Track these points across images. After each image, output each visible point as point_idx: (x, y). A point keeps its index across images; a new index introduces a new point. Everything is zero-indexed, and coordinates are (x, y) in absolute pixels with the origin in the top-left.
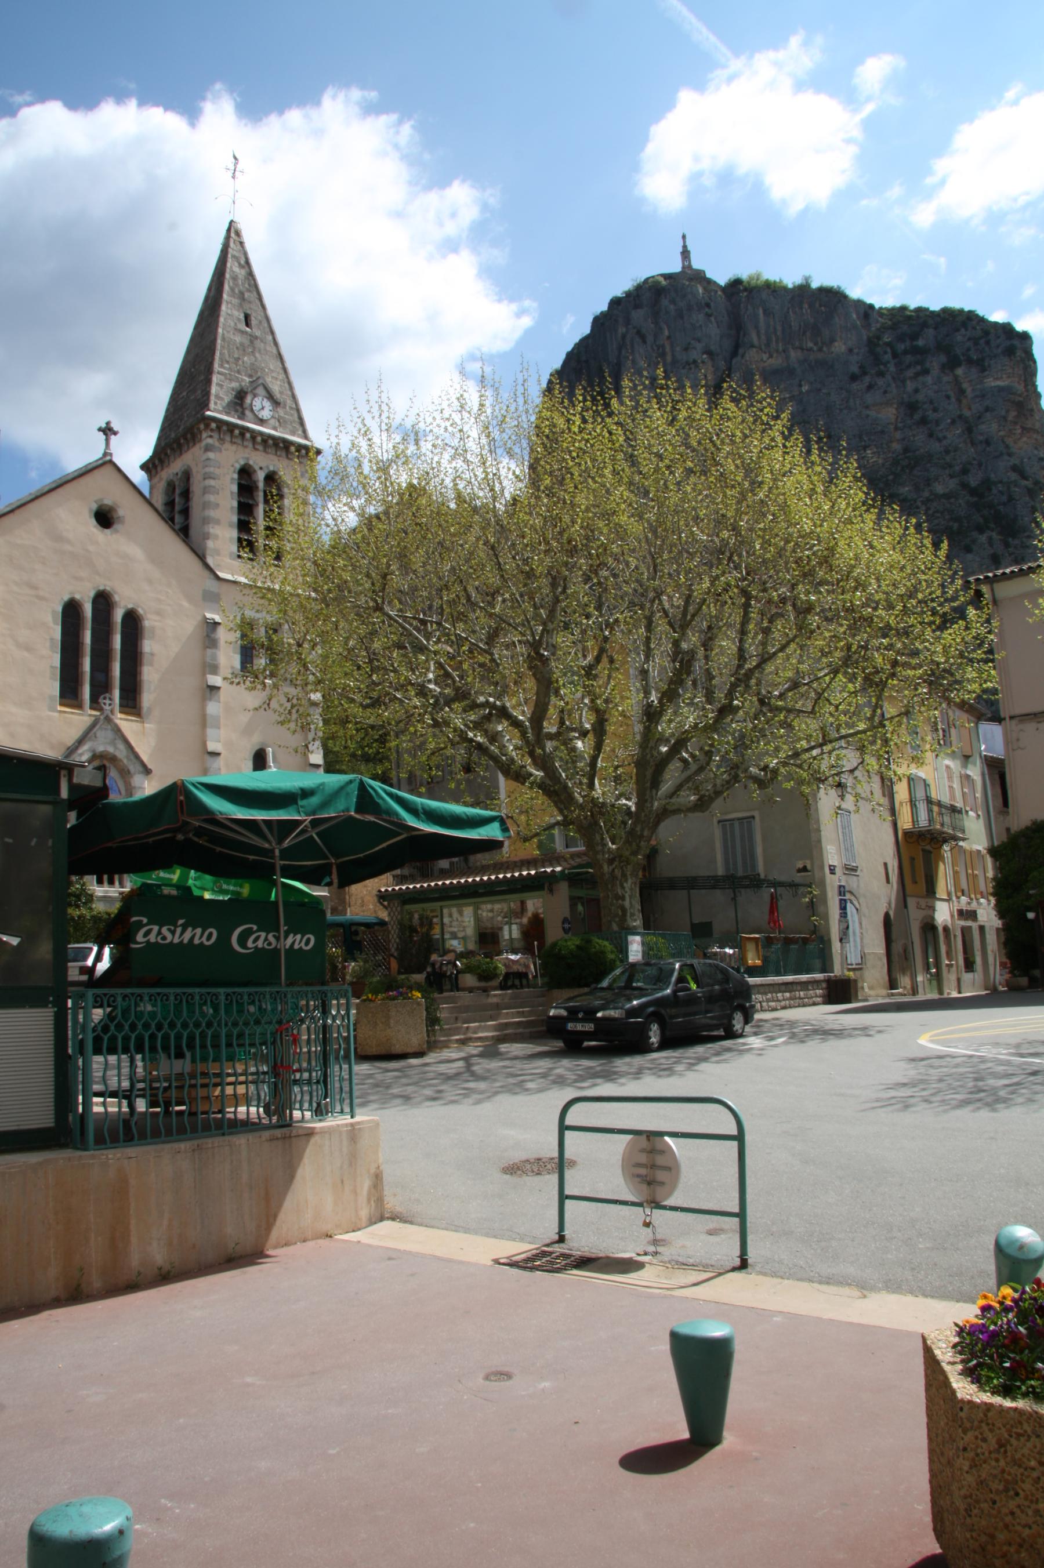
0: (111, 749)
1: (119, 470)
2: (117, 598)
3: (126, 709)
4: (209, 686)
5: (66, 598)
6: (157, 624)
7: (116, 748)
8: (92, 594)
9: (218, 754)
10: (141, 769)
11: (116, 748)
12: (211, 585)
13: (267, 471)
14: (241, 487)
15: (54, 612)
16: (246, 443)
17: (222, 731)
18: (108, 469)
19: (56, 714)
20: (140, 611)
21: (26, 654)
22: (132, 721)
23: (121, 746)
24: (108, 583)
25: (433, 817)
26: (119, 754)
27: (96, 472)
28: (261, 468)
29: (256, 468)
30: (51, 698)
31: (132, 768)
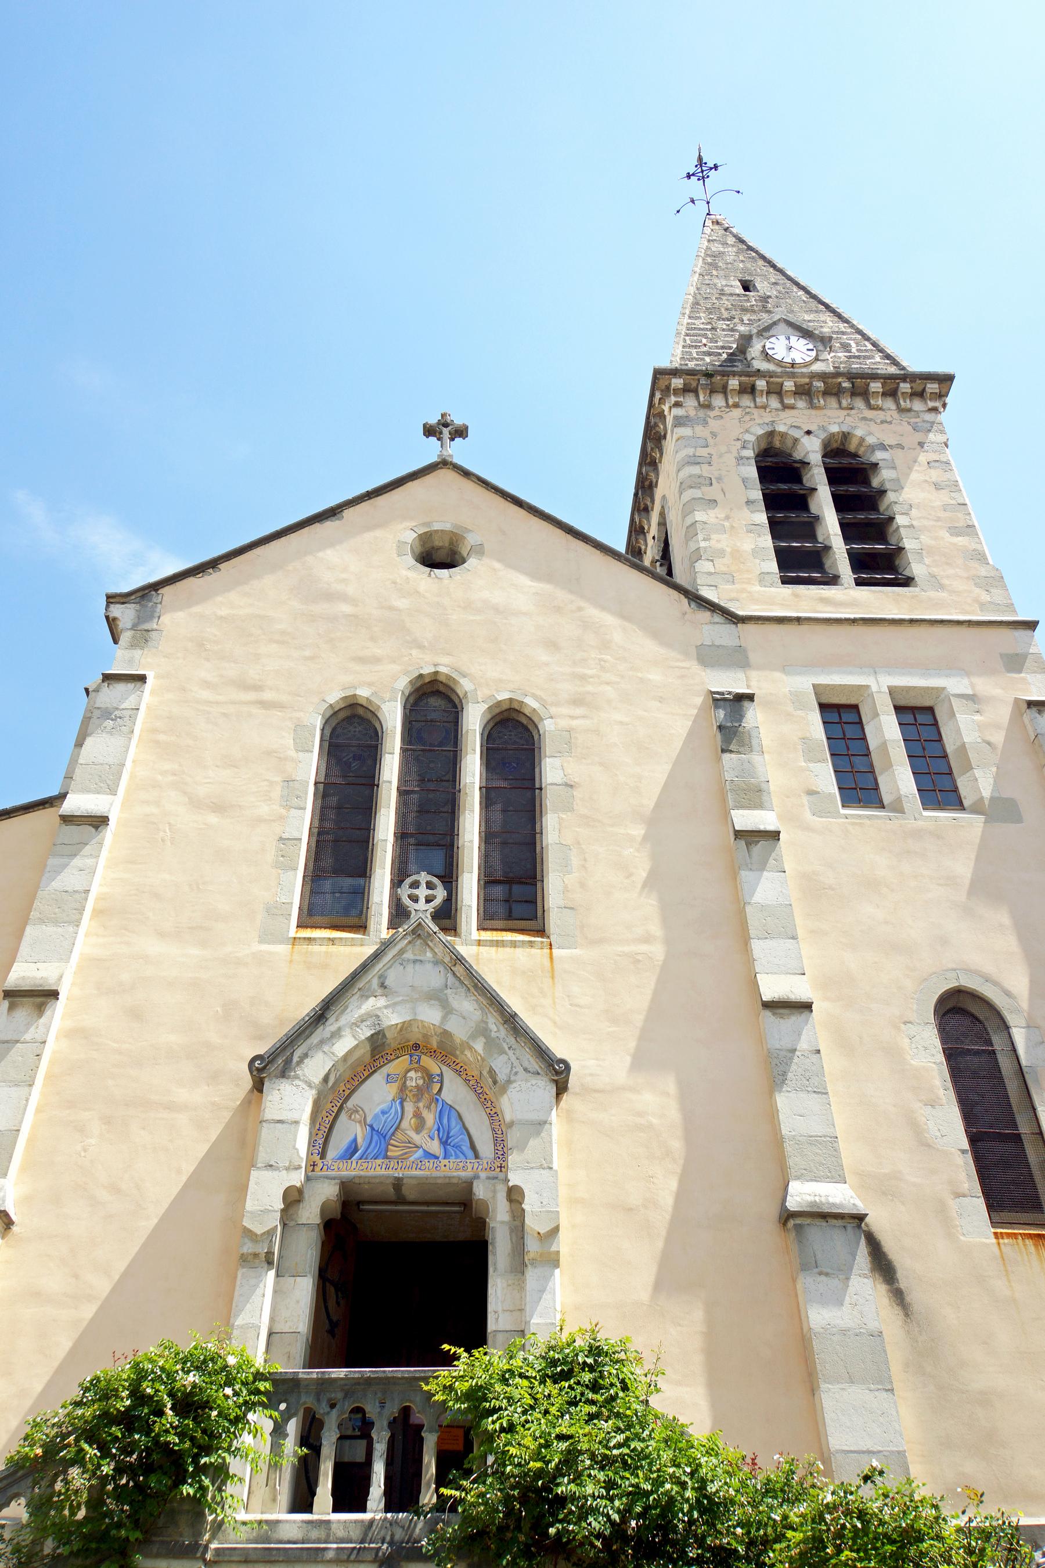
0: (430, 1015)
1: (466, 474)
2: (465, 685)
3: (1006, 1216)
4: (739, 834)
5: (334, 697)
6: (575, 723)
7: (448, 1010)
8: (403, 684)
9: (807, 1006)
10: (534, 1064)
11: (448, 1010)
12: (723, 634)
13: (823, 436)
14: (772, 502)
15: (299, 728)
16: (761, 400)
17: (806, 949)
18: (444, 474)
19: (283, 949)
20: (531, 703)
21: (213, 819)
22: (514, 944)
23: (467, 1005)
24: (445, 660)
25: (374, 1149)
26: (459, 1030)
27: (411, 486)
28: (809, 433)
29: (796, 434)
30: (276, 911)
31: (501, 1065)
